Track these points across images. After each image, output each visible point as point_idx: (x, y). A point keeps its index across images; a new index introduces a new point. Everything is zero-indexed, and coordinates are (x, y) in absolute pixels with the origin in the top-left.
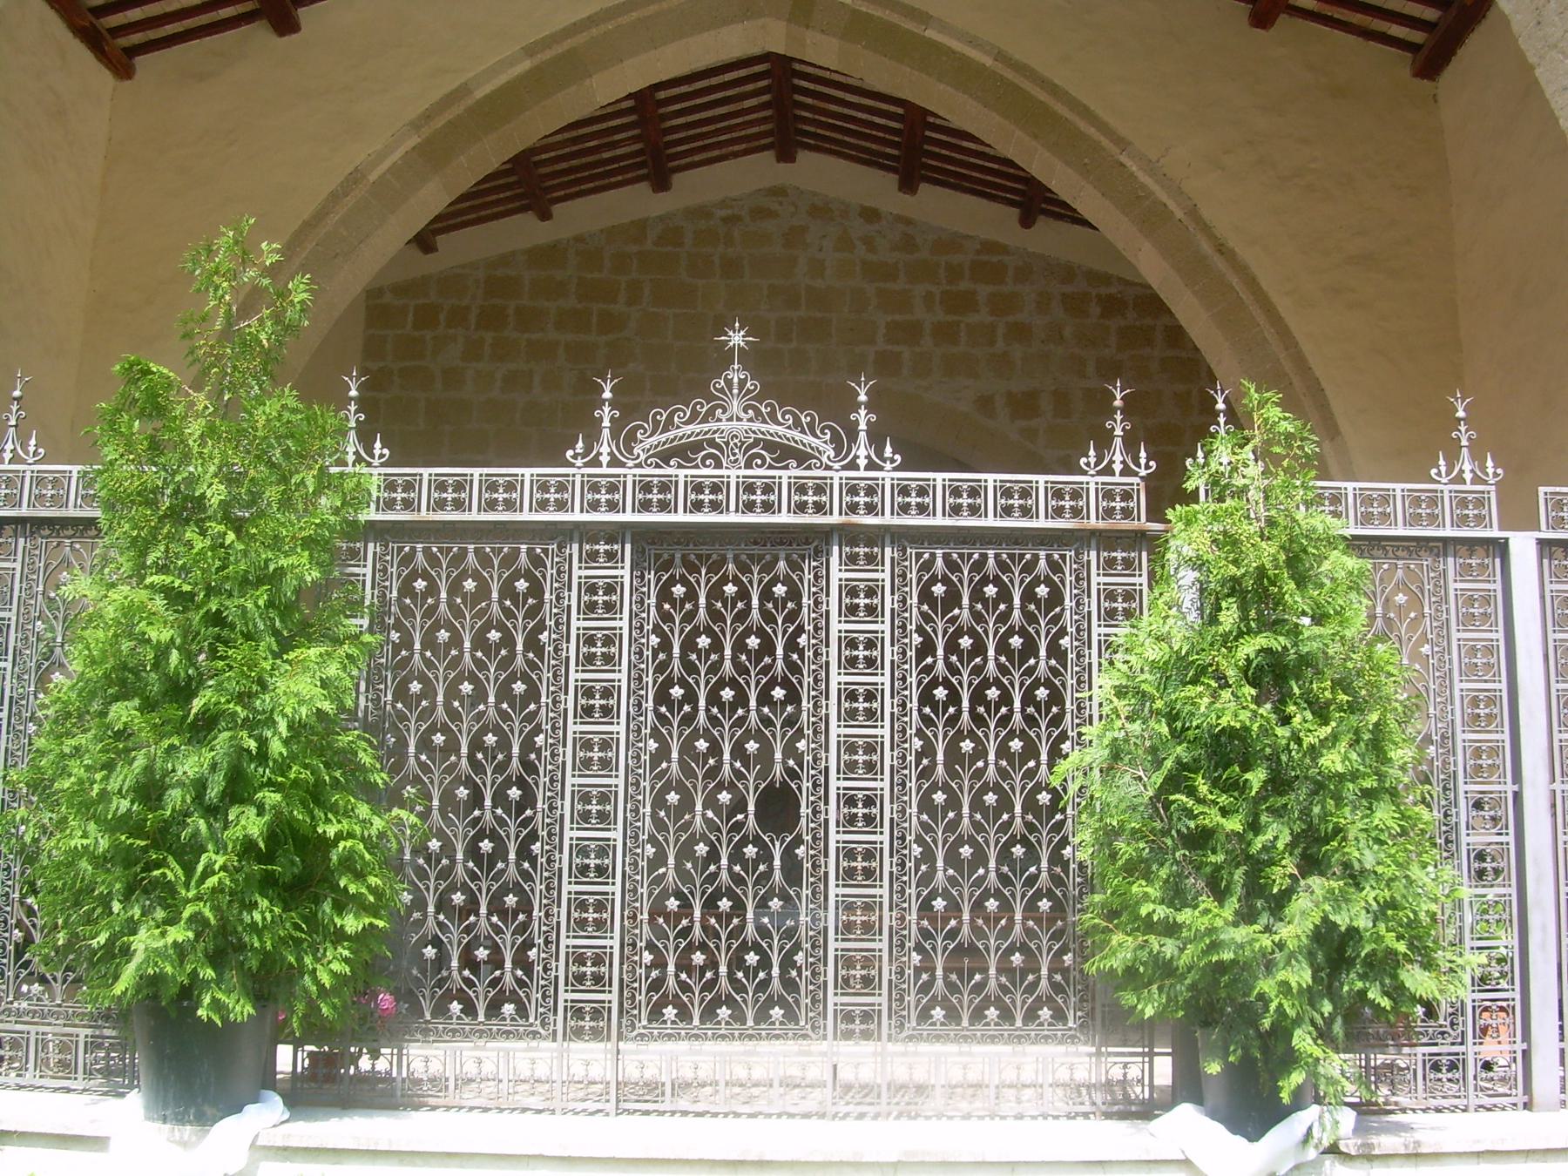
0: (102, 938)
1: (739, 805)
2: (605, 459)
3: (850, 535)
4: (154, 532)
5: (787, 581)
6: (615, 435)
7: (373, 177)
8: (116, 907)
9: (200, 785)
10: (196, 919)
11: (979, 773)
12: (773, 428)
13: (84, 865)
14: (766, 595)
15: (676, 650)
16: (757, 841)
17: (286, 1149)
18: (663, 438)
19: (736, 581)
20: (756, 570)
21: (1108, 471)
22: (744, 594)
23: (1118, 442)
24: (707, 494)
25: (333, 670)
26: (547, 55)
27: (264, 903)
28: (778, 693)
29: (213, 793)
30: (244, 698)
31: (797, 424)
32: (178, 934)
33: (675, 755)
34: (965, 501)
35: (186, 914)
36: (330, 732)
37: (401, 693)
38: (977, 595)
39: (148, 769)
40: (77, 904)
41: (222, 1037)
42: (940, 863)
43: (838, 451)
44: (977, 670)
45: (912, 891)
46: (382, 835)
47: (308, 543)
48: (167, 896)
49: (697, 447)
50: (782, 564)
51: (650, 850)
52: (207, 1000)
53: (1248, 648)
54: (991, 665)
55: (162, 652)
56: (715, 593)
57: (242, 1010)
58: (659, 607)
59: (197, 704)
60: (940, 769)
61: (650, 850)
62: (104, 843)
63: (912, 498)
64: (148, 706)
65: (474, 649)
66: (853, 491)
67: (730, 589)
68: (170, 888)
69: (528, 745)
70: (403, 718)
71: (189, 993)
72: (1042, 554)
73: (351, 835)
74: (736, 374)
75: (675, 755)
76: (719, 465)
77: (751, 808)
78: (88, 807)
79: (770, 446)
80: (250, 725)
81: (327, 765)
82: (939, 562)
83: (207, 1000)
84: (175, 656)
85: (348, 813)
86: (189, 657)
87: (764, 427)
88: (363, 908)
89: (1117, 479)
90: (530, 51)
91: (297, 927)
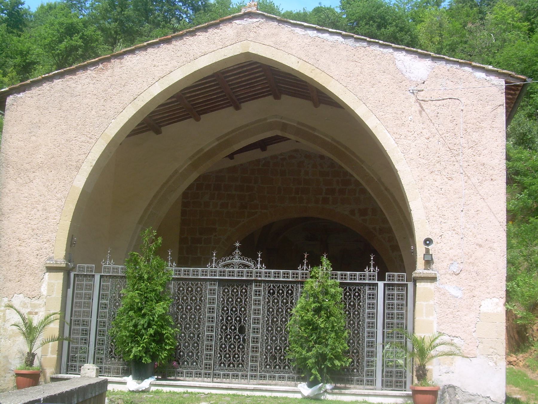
0: (127, 349)
1: (235, 329)
2: (214, 267)
3: (256, 281)
4: (136, 283)
5: (245, 289)
6: (216, 262)
7: (180, 171)
8: (130, 344)
9: (143, 325)
10: (143, 347)
11: (277, 324)
12: (243, 261)
13: (125, 338)
14: (241, 292)
15: (225, 301)
16: (238, 335)
17: (155, 384)
18: (224, 263)
19: (236, 289)
20: (240, 287)
21: (303, 270)
22: (237, 291)
23: (305, 264)
24: (231, 273)
25: (165, 306)
26: (222, 140)
27: (153, 344)
28: (243, 309)
29: (145, 326)
30: (151, 311)
31: (248, 260)
32: (140, 348)
33: (225, 320)
34: (277, 275)
35: (141, 346)
36: (164, 316)
37: (178, 308)
38: (278, 292)
39: (135, 322)
40: (123, 344)
41: (146, 365)
42: (269, 340)
43: (255, 266)
44: (277, 306)
45: (264, 345)
46: (173, 333)
47: (161, 284)
48: (138, 343)
49: (230, 265)
50: (244, 286)
51: (220, 337)
52: (144, 359)
53: (313, 306)
54: (280, 305)
55: (138, 303)
56: (233, 291)
57: (149, 361)
58: (223, 293)
59: (143, 312)
60: (270, 323)
61: (220, 337)
62: (128, 334)
63: (268, 275)
64: (135, 312)
65: (190, 300)
66: (257, 273)
67: (235, 290)
68: (138, 341)
69: (199, 318)
70: (178, 312)
71: (141, 358)
72: (290, 285)
73: (167, 333)
74: (237, 251)
75: (225, 320)
76: (234, 268)
77: (237, 330)
78: (125, 328)
79: (243, 265)
80: (151, 315)
81: (164, 321)
82: (272, 286)
83: (144, 359)
84: (139, 304)
85: (167, 329)
86: (141, 303)
87: (242, 261)
88: (170, 345)
89: (304, 271)
90: (218, 139)
91: (158, 348)
